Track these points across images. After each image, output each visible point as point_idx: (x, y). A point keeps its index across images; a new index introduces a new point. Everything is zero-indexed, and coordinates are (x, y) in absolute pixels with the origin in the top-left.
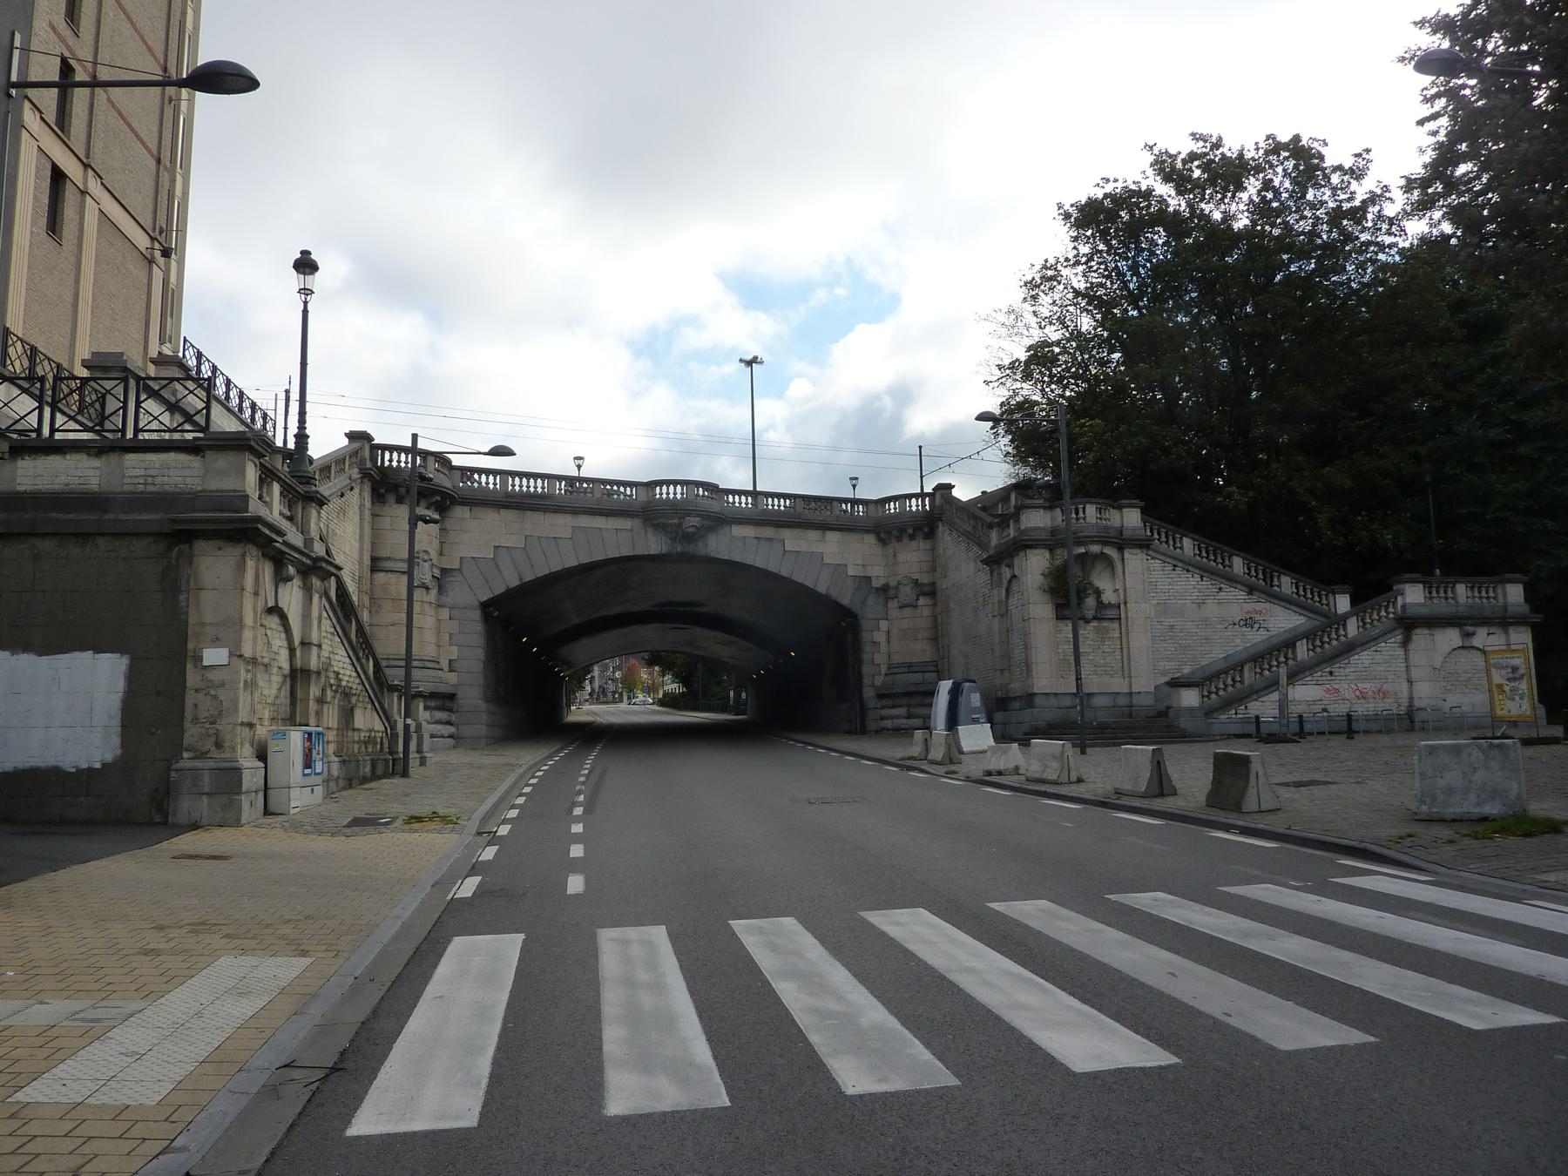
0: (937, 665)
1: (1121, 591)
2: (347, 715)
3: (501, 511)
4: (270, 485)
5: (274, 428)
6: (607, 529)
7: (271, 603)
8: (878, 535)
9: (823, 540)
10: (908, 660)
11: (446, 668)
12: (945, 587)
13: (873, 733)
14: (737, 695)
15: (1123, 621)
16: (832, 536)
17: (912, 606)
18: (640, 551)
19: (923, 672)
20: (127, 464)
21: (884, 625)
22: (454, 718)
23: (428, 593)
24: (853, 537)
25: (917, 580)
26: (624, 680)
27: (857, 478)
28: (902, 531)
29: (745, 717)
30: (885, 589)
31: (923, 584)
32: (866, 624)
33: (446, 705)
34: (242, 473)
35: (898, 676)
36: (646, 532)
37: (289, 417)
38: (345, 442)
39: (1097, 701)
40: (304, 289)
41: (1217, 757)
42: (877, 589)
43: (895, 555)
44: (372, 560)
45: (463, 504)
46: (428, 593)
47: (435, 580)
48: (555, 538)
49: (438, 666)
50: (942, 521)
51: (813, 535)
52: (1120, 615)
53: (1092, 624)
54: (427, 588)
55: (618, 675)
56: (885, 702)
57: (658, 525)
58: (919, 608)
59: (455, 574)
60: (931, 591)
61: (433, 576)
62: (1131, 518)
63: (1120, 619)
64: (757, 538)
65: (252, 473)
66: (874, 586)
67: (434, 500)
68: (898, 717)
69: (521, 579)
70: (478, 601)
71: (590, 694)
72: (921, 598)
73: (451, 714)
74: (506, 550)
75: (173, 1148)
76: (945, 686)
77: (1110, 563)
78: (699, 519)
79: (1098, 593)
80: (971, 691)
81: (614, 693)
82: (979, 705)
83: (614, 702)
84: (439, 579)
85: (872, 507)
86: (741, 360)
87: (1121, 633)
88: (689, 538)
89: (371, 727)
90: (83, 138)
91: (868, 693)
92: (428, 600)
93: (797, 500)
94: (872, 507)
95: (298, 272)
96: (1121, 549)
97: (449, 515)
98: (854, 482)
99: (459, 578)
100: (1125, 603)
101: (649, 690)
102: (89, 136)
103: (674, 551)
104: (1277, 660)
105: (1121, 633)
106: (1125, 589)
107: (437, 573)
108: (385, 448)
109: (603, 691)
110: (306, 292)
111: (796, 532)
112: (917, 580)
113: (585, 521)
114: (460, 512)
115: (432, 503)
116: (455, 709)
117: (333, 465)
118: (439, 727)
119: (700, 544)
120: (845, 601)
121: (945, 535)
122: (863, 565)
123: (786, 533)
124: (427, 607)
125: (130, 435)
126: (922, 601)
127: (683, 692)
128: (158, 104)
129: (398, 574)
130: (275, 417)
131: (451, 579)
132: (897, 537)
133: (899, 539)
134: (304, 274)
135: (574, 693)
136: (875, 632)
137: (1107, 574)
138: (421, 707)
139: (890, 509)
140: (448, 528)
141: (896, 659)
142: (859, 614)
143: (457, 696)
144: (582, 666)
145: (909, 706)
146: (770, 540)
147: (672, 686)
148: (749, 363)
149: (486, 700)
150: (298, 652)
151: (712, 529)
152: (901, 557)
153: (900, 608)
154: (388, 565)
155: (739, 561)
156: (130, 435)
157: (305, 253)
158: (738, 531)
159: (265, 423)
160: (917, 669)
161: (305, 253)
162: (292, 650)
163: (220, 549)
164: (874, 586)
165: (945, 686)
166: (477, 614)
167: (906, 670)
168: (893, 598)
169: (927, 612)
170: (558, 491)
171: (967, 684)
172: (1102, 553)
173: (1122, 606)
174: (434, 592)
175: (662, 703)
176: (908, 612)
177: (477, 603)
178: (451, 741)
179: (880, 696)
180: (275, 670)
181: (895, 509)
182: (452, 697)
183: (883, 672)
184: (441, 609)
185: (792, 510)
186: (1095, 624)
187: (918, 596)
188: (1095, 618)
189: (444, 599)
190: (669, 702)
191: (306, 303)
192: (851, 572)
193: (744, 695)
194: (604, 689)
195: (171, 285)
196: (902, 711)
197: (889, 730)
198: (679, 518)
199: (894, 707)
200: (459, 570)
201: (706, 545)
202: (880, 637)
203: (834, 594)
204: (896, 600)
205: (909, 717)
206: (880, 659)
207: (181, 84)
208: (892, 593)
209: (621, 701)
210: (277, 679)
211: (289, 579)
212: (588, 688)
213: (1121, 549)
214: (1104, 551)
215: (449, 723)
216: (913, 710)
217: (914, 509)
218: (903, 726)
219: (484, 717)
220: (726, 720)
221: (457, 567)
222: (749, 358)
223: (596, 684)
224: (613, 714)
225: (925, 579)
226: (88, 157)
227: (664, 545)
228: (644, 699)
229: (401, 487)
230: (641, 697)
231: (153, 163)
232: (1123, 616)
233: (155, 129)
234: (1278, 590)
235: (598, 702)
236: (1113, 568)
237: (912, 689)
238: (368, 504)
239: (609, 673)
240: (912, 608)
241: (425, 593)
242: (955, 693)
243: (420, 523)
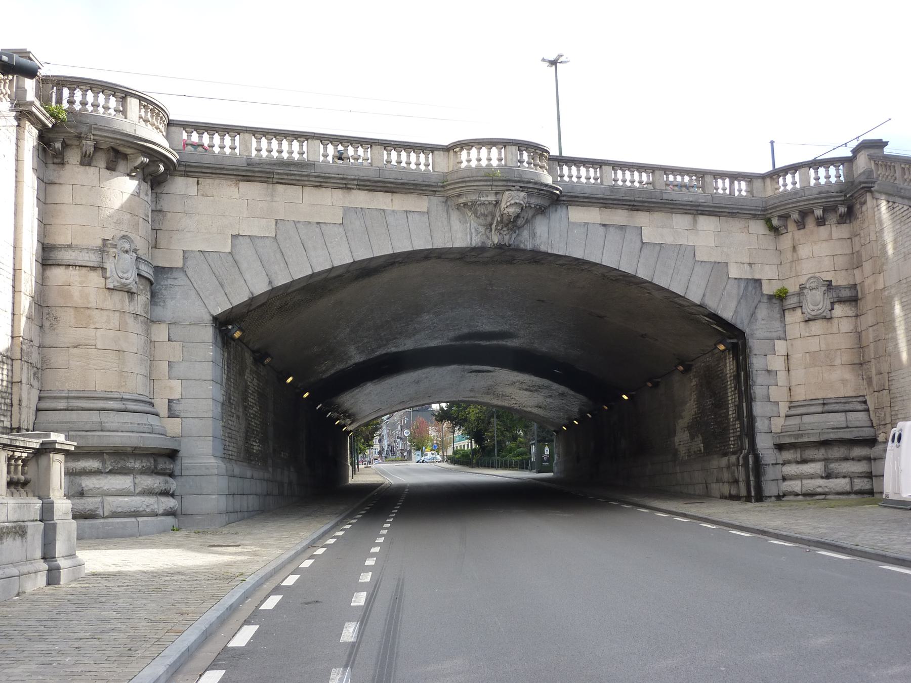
0: (865, 402)
3: (242, 184)
6: (393, 211)
8: (768, 221)
9: (694, 228)
10: (820, 395)
11: (164, 411)
12: (881, 286)
13: (773, 499)
14: (540, 451)
16: (707, 224)
17: (825, 318)
18: (440, 242)
19: (846, 411)
21: (780, 346)
22: (173, 485)
23: (131, 299)
24: (735, 225)
25: (831, 281)
26: (412, 438)
28: (805, 214)
29: (552, 474)
30: (780, 297)
31: (838, 287)
32: (756, 345)
33: (160, 467)
35: (806, 419)
36: (449, 217)
41: (50, 438)
42: (771, 297)
43: (794, 248)
44: (43, 249)
45: (187, 174)
46: (131, 299)
47: (143, 281)
48: (318, 223)
49: (147, 408)
50: (871, 192)
51: (681, 221)
54: (131, 293)
55: (406, 433)
56: (788, 455)
57: (465, 204)
58: (835, 321)
59: (175, 275)
64: (604, 225)
66: (765, 292)
67: (139, 162)
68: (812, 477)
69: (270, 283)
70: (211, 315)
71: (380, 453)
72: (836, 306)
73: (170, 480)
74: (248, 240)
75: (217, 660)
78: (523, 194)
81: (402, 451)
83: (403, 459)
85: (758, 184)
91: (764, 443)
92: (131, 309)
93: (657, 172)
94: (758, 184)
97: (166, 190)
99: (181, 280)
101: (440, 447)
103: (489, 243)
108: (61, 82)
109: (393, 450)
111: (658, 217)
112: (831, 281)
113: (361, 199)
114: (181, 186)
115: (136, 168)
116: (177, 473)
118: (151, 500)
119: (525, 233)
120: (727, 314)
122: (750, 264)
123: (642, 219)
124: (130, 320)
126: (839, 310)
127: (475, 449)
129: (84, 270)
131: (170, 282)
132: (797, 222)
135: (362, 451)
136: (769, 357)
140: (165, 209)
141: (801, 394)
142: (747, 331)
143: (180, 454)
144: (366, 420)
145: (826, 460)
146: (622, 228)
147: (465, 444)
148: (554, 63)
149: (226, 457)
151: (541, 211)
152: (804, 251)
154: (67, 257)
155: (581, 257)
158: (577, 215)
160: (837, 407)
164: (765, 292)
166: (208, 333)
167: (819, 409)
168: (794, 309)
169: (846, 326)
170: (322, 158)
174: (142, 299)
175: (453, 460)
177: (208, 318)
178: (170, 520)
179: (780, 447)
182: (172, 455)
183: (783, 414)
184: (155, 327)
185: (650, 187)
187: (832, 303)
189: (159, 312)
190: (461, 459)
192: (734, 272)
193: (547, 450)
194: (393, 447)
196: (816, 468)
197: (797, 495)
198: (496, 194)
199: (804, 461)
200: (182, 270)
201: (533, 235)
202: (776, 364)
203: (713, 305)
204: (799, 311)
205: (828, 476)
208: (791, 301)
209: (410, 458)
212: (377, 447)
215: (166, 493)
216: (832, 466)
217: (823, 181)
218: (820, 490)
219: (222, 483)
220: (535, 479)
221: (180, 265)
223: (385, 443)
224: (401, 472)
227: (474, 234)
228: (433, 456)
229: (86, 138)
230: (429, 455)
235: (387, 459)
237: (832, 436)
239: (398, 432)
240: (825, 322)
241: (127, 300)
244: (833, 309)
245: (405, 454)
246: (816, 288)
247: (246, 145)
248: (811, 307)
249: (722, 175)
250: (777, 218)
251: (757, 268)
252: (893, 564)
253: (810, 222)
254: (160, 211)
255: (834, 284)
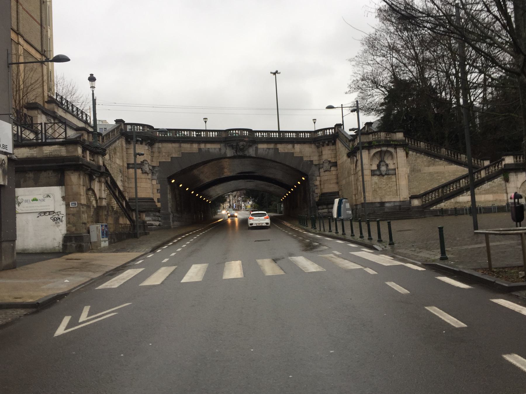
1: (396, 164)
2: (117, 220)
4: (86, 152)
5: (90, 119)
7: (89, 187)
15: (397, 175)
20: (44, 149)
23: (148, 175)
27: (315, 120)
34: (77, 150)
37: (97, 106)
38: (114, 123)
39: (387, 205)
40: (92, 87)
46: (148, 175)
52: (396, 172)
53: (385, 176)
54: (148, 174)
60: (335, 164)
61: (149, 169)
62: (400, 136)
63: (395, 174)
65: (80, 150)
76: (337, 201)
77: (391, 153)
79: (387, 165)
80: (346, 202)
82: (349, 207)
84: (152, 170)
86: (271, 73)
87: (396, 179)
88: (242, 150)
89: (125, 223)
90: (16, 24)
95: (90, 81)
96: (395, 148)
98: (314, 121)
100: (398, 168)
102: (18, 23)
104: (453, 187)
105: (396, 179)
106: (397, 163)
107: (151, 168)
110: (93, 87)
117: (111, 133)
121: (339, 144)
124: (148, 180)
125: (44, 141)
126: (333, 169)
128: (39, 4)
130: (90, 115)
132: (322, 145)
133: (323, 146)
134: (92, 81)
137: (390, 158)
138: (144, 215)
139: (319, 134)
148: (275, 74)
150: (99, 201)
153: (324, 172)
156: (44, 141)
157: (92, 75)
159: (87, 117)
161: (92, 75)
162: (97, 201)
163: (72, 173)
165: (337, 201)
171: (344, 200)
172: (387, 150)
173: (396, 169)
174: (150, 175)
176: (327, 173)
180: (92, 207)
181: (321, 134)
186: (386, 176)
187: (331, 167)
188: (386, 174)
191: (93, 91)
195: (50, 70)
202: (318, 183)
206: (318, 191)
207: (52, 61)
210: (92, 210)
211: (94, 180)
213: (395, 148)
214: (388, 149)
222: (274, 71)
225: (333, 160)
226: (18, 30)
231: (39, 27)
232: (397, 173)
233: (39, 14)
234: (460, 160)
236: (392, 155)
238: (124, 145)
242: (340, 203)
243: (138, 156)
244: (331, 168)
245: (239, 207)
246: (326, 163)
247: (190, 134)
248: (325, 168)
249: (302, 132)
250: (220, 147)
251: (311, 157)
252: (6, 270)
253: (325, 145)
254: (153, 152)
255: (331, 161)
